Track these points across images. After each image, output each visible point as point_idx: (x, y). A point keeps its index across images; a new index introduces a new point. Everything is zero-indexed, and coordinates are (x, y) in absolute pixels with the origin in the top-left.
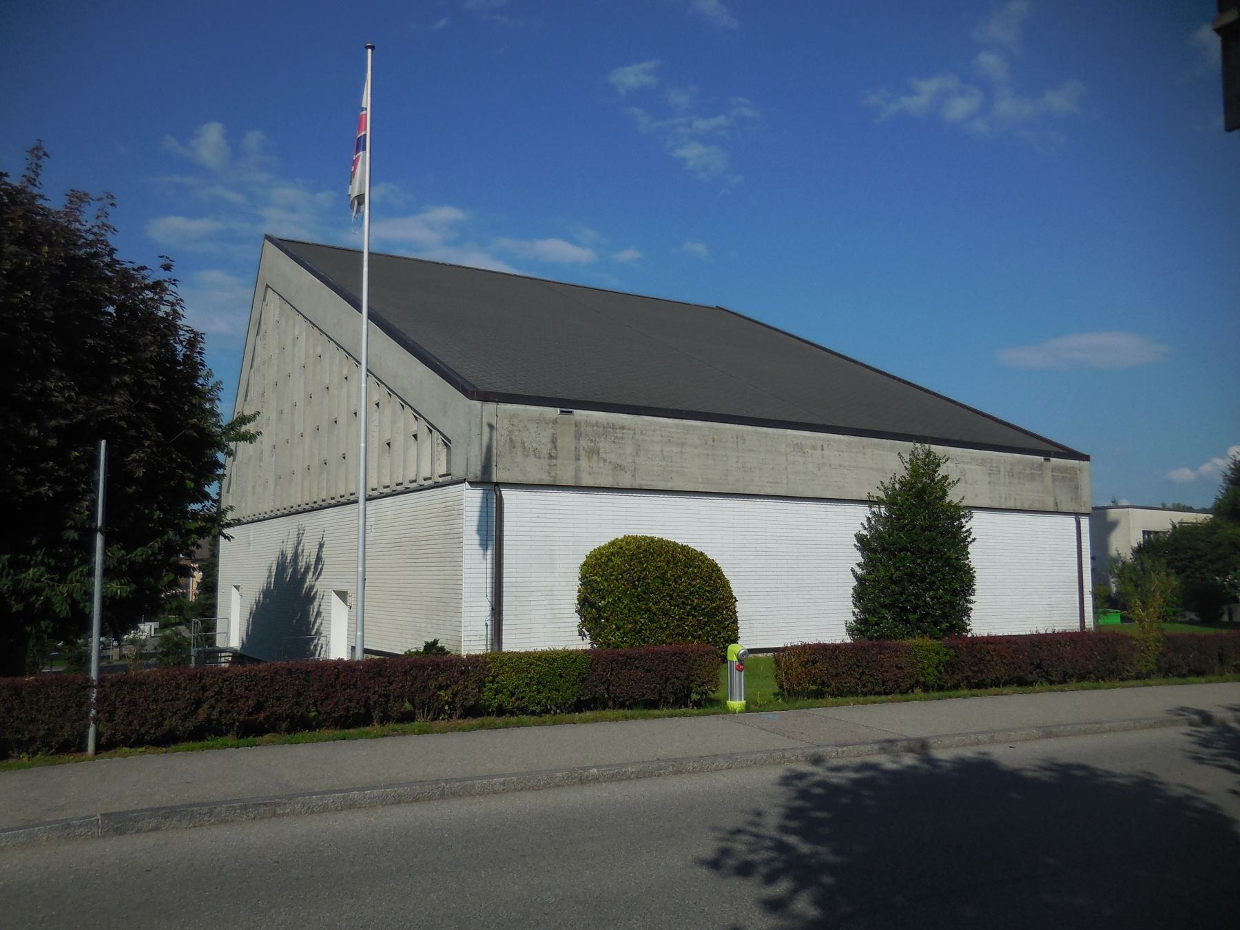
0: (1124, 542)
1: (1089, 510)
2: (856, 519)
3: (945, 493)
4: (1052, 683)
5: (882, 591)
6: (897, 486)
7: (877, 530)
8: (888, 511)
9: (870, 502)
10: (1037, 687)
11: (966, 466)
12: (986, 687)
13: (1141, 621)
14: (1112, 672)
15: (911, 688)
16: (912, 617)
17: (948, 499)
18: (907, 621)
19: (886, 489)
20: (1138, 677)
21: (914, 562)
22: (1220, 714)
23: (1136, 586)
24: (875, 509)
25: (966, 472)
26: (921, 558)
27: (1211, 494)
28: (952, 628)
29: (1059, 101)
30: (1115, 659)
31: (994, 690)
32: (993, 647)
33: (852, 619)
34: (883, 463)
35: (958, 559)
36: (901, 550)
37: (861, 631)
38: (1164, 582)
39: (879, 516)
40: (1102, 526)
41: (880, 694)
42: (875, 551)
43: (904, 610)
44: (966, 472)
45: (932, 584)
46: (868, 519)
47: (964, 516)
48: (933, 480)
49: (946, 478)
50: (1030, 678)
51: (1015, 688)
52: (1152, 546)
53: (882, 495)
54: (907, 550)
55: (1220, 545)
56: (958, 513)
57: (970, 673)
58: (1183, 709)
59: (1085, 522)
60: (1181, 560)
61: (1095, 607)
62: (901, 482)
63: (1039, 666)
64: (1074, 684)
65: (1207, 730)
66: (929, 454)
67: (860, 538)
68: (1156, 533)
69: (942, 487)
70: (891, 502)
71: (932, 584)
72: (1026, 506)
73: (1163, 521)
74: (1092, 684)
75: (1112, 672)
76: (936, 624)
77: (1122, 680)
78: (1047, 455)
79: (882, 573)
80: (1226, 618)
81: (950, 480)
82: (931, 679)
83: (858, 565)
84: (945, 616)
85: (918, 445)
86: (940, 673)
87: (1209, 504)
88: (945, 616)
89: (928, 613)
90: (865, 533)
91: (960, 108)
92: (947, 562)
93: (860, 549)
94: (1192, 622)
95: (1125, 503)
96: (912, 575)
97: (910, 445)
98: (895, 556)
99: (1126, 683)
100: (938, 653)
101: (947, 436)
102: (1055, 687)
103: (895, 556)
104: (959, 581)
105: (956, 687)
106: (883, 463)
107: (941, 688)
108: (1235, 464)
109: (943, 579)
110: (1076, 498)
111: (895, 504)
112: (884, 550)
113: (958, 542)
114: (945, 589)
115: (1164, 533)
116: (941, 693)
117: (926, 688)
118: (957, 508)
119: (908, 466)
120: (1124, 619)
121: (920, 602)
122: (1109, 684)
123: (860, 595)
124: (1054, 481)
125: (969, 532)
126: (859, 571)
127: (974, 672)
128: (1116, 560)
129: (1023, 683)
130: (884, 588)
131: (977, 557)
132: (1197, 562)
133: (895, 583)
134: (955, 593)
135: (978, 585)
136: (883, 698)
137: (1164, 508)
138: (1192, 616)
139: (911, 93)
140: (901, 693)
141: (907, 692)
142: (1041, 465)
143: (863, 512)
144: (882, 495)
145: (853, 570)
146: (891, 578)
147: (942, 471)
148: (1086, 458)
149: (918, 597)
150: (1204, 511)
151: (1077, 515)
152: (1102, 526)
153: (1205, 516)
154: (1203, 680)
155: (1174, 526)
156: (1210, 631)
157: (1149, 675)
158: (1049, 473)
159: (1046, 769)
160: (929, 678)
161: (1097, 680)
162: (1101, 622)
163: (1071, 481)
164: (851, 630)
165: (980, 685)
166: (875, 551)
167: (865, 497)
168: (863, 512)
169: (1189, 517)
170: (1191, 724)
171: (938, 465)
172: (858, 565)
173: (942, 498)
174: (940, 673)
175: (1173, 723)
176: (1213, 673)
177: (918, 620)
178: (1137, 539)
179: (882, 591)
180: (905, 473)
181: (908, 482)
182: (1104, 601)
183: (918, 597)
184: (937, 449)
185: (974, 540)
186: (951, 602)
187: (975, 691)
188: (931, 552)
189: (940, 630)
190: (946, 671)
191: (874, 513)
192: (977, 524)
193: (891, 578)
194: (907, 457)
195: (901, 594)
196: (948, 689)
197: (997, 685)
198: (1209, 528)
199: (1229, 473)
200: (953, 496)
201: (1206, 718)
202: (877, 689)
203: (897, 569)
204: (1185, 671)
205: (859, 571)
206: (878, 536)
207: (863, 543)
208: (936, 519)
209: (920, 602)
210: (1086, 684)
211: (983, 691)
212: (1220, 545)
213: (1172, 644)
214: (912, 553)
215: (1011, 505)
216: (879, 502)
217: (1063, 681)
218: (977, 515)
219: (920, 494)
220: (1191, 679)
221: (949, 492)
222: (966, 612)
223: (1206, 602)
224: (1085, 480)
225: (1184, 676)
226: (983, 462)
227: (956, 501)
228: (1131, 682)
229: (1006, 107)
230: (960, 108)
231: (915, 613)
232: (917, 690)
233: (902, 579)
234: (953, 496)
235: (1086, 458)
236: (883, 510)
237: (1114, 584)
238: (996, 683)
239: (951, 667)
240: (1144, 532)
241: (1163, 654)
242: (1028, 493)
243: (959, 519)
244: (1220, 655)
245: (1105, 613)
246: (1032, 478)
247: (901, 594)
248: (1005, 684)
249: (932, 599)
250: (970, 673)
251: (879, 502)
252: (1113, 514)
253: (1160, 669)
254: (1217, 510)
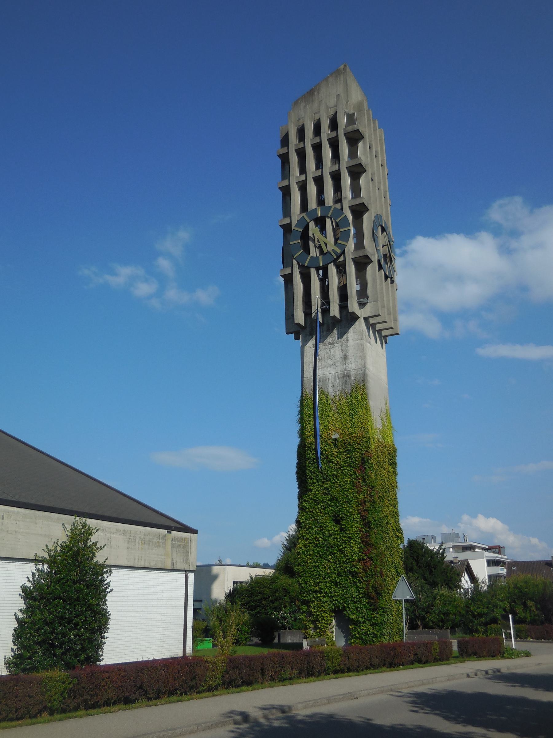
0: (220, 591)
1: (194, 568)
2: (23, 574)
3: (94, 555)
4: (149, 699)
5: (37, 631)
6: (59, 549)
7: (38, 583)
8: (49, 567)
9: (36, 561)
10: (138, 704)
11: (112, 536)
12: (100, 707)
13: (222, 646)
14: (192, 687)
15: (40, 712)
16: (59, 651)
17: (95, 560)
18: (55, 655)
19: (49, 552)
20: (209, 690)
21: (64, 607)
22: (255, 713)
23: (221, 621)
24: (40, 566)
25: (110, 540)
26: (70, 604)
27: (274, 556)
28: (88, 659)
29: (205, 296)
30: (194, 678)
31: (106, 709)
32: (107, 675)
33: (9, 654)
34: (50, 531)
35: (98, 605)
36: (55, 599)
37: (16, 665)
38: (239, 617)
39: (43, 571)
40: (204, 576)
41: (12, 720)
42: (34, 599)
43: (52, 645)
44: (110, 540)
45: (76, 624)
46: (33, 574)
47: (106, 572)
48: (86, 545)
49: (95, 544)
50: (133, 697)
51: (122, 706)
52: (238, 593)
53: (46, 556)
54: (60, 598)
55: (277, 590)
56: (101, 570)
57: (88, 697)
58: (232, 712)
59: (191, 576)
60: (254, 601)
61: (194, 637)
62: (62, 546)
63: (141, 687)
64: (165, 699)
65: (245, 726)
66: (84, 526)
67: (24, 589)
68: (241, 583)
69: (93, 549)
70: (52, 562)
71: (76, 624)
72: (152, 565)
73: (244, 575)
74: (178, 698)
75: (192, 687)
76: (76, 656)
77: (199, 693)
78: (169, 529)
79: (39, 616)
80: (276, 641)
81: (98, 546)
82: (56, 704)
83: (20, 610)
84: (83, 650)
85: (78, 518)
86: (64, 698)
87: (273, 562)
88: (83, 650)
89: (71, 648)
90: (29, 585)
91: (144, 289)
92: (90, 607)
93: (23, 598)
94: (256, 645)
95: (228, 561)
96: (62, 618)
97: (69, 519)
98: (50, 603)
99: (201, 695)
100: (64, 683)
101: (100, 513)
102: (150, 703)
103: (50, 603)
104: (97, 621)
105: (76, 709)
106: (50, 531)
107: (64, 711)
108: (289, 537)
109: (85, 620)
110: (187, 560)
111: (55, 563)
112: (42, 598)
113: (98, 590)
114: (86, 629)
115: (246, 583)
116: (63, 715)
117: (52, 712)
118: (102, 566)
119: (69, 534)
120: (214, 645)
121: (66, 640)
122: (189, 697)
123: (20, 635)
124: (173, 547)
125: (108, 585)
126: (20, 615)
127: (92, 695)
128: (216, 601)
129: (128, 701)
130: (39, 628)
131: (113, 604)
132: (264, 602)
133: (48, 624)
134: (93, 631)
135: (112, 624)
136: (14, 723)
137: (248, 566)
138: (256, 640)
139: (116, 274)
140: (30, 717)
141: (35, 716)
142: (165, 536)
143: (29, 569)
144: (48, 558)
145: (15, 615)
146: (45, 620)
147: (93, 539)
148: (195, 532)
149: (64, 635)
150: (266, 566)
151: (186, 571)
152: (204, 576)
153: (270, 571)
154: (250, 688)
155: (252, 578)
156: (265, 651)
157: (216, 688)
158: (170, 542)
159: (411, 694)
160: (55, 703)
161: (181, 695)
162: (199, 647)
163: (184, 547)
164: (8, 664)
165: (96, 706)
166: (34, 599)
167: (32, 557)
168: (29, 569)
169: (261, 572)
170: (236, 723)
171: (91, 534)
172: (20, 610)
173: (92, 559)
174: (64, 698)
175: (224, 724)
176: (257, 682)
177: (63, 654)
178: (229, 587)
179: (37, 631)
180: (66, 539)
181: (67, 546)
182: (203, 631)
183: (64, 635)
184: (91, 522)
185: (111, 590)
186: (89, 638)
187: (91, 711)
188: (78, 599)
189: (79, 661)
190: (69, 697)
191: (38, 570)
192: (116, 580)
193: (45, 620)
194: (69, 527)
195: (52, 633)
196: (70, 711)
197: (108, 705)
198: (273, 579)
199: (285, 543)
200: (99, 558)
201: (245, 717)
202: (10, 716)
203: (50, 613)
204: (240, 682)
205: (20, 615)
206: (38, 587)
207: (26, 593)
208: (85, 575)
209: (66, 640)
210: (174, 698)
211: (96, 710)
212: (277, 590)
213: (233, 663)
214: (64, 601)
215: (142, 564)
216: (43, 561)
217: (158, 698)
218: (115, 571)
219: (75, 556)
220: (244, 688)
221: (97, 554)
222: (99, 646)
223: (265, 631)
224: (193, 548)
225: (239, 686)
226: (124, 533)
227: (101, 561)
228: (205, 694)
229: (172, 294)
230: (144, 289)
231: (61, 648)
232: (45, 714)
233: (53, 621)
234: (99, 558)
235: (195, 532)
236: (46, 567)
237: (206, 621)
238: (107, 703)
239: (73, 693)
240: (234, 582)
241: (227, 672)
242: (154, 556)
243: (102, 575)
244: (262, 669)
245: (202, 641)
246: (158, 545)
247: (52, 633)
248: (114, 703)
249: (75, 636)
250: (88, 697)
251: (43, 561)
252: (215, 570)
253: (224, 683)
254: (277, 567)
